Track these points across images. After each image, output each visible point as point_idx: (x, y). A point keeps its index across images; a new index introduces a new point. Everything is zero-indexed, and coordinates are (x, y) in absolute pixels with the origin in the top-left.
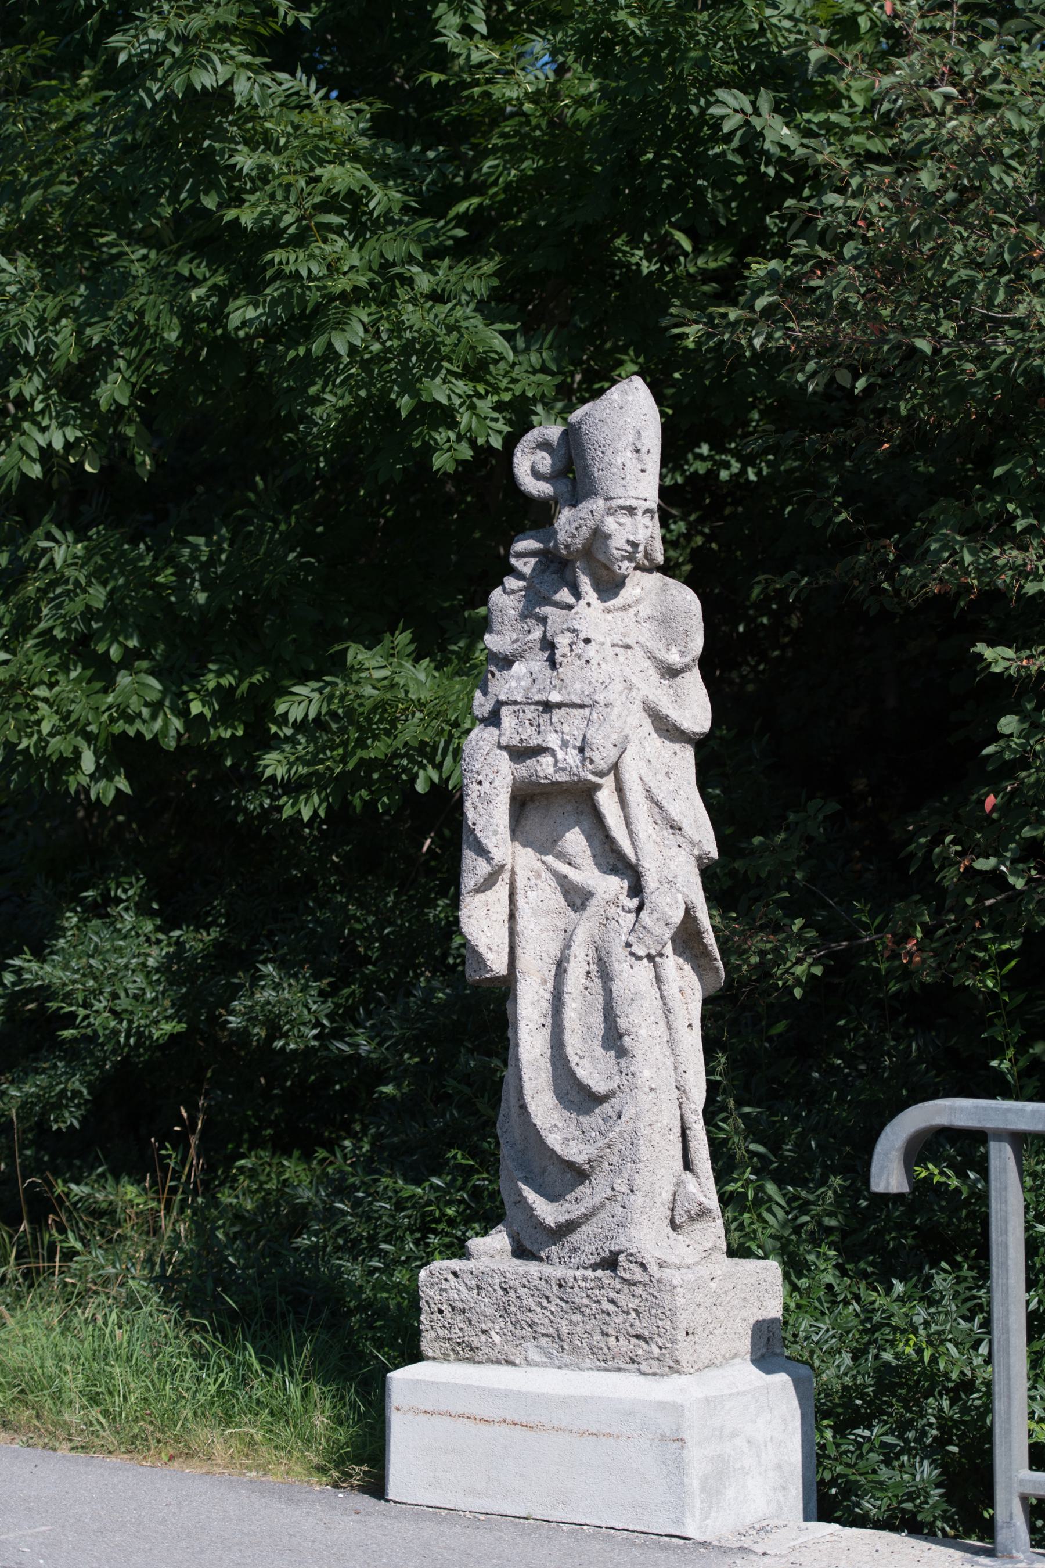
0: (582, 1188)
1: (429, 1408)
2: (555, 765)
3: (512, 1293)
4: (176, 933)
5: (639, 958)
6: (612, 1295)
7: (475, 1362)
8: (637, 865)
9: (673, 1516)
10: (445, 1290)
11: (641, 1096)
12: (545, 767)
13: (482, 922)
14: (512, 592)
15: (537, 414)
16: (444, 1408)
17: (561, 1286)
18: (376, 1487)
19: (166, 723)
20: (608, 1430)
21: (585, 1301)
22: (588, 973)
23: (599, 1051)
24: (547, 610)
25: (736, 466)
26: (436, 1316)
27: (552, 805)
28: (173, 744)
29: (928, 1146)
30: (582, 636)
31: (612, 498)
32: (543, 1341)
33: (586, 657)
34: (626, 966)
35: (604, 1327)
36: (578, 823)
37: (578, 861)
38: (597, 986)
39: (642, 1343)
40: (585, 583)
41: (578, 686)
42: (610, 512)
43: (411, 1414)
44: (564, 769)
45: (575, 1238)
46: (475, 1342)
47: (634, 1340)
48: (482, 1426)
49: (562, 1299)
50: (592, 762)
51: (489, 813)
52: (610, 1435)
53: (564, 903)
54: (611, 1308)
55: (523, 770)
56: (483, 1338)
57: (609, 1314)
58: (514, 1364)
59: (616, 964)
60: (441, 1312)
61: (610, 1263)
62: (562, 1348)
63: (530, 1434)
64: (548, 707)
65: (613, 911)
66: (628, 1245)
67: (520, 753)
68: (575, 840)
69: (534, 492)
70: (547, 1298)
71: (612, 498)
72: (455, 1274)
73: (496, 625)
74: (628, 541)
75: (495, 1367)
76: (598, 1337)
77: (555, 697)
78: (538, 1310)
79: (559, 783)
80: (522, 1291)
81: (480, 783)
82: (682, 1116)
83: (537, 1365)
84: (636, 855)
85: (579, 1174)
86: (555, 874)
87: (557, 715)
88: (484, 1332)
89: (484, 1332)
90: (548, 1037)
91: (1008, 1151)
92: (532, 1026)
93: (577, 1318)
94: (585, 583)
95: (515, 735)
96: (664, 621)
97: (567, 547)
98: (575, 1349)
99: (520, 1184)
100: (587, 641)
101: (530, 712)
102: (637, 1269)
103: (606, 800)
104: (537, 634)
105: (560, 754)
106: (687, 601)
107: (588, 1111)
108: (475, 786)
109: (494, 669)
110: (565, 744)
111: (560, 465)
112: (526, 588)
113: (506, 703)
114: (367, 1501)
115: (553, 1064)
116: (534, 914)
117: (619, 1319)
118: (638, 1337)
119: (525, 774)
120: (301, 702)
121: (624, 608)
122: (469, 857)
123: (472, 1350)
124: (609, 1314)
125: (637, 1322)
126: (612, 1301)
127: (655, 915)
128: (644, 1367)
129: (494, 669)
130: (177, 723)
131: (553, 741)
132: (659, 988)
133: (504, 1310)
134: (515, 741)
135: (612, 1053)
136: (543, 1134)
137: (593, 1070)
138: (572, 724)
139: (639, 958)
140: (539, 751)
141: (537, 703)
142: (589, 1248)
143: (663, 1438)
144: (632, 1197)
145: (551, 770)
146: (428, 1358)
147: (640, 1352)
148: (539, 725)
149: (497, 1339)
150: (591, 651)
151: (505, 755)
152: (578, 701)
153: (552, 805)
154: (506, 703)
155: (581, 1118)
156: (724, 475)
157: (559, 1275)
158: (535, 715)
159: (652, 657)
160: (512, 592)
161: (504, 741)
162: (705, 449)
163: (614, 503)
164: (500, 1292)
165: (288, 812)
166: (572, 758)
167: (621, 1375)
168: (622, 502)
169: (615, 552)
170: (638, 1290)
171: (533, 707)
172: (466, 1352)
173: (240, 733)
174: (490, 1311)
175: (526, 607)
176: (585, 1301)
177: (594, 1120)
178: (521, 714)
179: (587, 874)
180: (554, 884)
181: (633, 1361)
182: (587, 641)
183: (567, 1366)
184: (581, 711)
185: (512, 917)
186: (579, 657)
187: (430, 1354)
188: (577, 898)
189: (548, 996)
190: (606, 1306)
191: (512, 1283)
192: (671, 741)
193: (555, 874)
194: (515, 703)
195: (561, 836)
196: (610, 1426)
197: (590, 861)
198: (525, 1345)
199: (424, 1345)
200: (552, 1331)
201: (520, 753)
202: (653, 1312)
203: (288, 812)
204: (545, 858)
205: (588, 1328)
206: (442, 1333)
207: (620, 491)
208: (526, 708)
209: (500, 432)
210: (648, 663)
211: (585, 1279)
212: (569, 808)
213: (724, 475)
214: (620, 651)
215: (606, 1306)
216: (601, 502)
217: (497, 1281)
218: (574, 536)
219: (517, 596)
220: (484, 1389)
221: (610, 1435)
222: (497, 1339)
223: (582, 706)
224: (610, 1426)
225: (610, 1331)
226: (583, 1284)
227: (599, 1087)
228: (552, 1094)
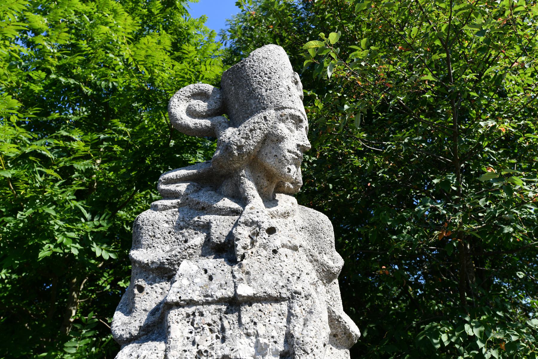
14: (165, 208)
15: (93, 247)
24: (205, 218)
30: (266, 226)
31: (283, 108)
40: (250, 187)
64: (234, 304)
71: (283, 108)
73: (146, 240)
74: (298, 145)
77: (244, 290)
87: (248, 313)
94: (250, 187)
95: (190, 347)
96: (314, 231)
97: (240, 148)
101: (210, 314)
104: (198, 239)
109: (142, 282)
112: (179, 205)
113: (177, 305)
129: (142, 282)
141: (220, 301)
148: (223, 330)
152: (274, 293)
154: (177, 305)
158: (216, 318)
159: (313, 260)
160: (165, 208)
163: (286, 112)
169: (288, 154)
171: (213, 307)
178: (198, 318)
184: (277, 306)
186: (265, 247)
192: (337, 347)
194: (190, 303)
208: (204, 309)
209: (77, 248)
216: (272, 111)
218: (247, 138)
223: (278, 300)
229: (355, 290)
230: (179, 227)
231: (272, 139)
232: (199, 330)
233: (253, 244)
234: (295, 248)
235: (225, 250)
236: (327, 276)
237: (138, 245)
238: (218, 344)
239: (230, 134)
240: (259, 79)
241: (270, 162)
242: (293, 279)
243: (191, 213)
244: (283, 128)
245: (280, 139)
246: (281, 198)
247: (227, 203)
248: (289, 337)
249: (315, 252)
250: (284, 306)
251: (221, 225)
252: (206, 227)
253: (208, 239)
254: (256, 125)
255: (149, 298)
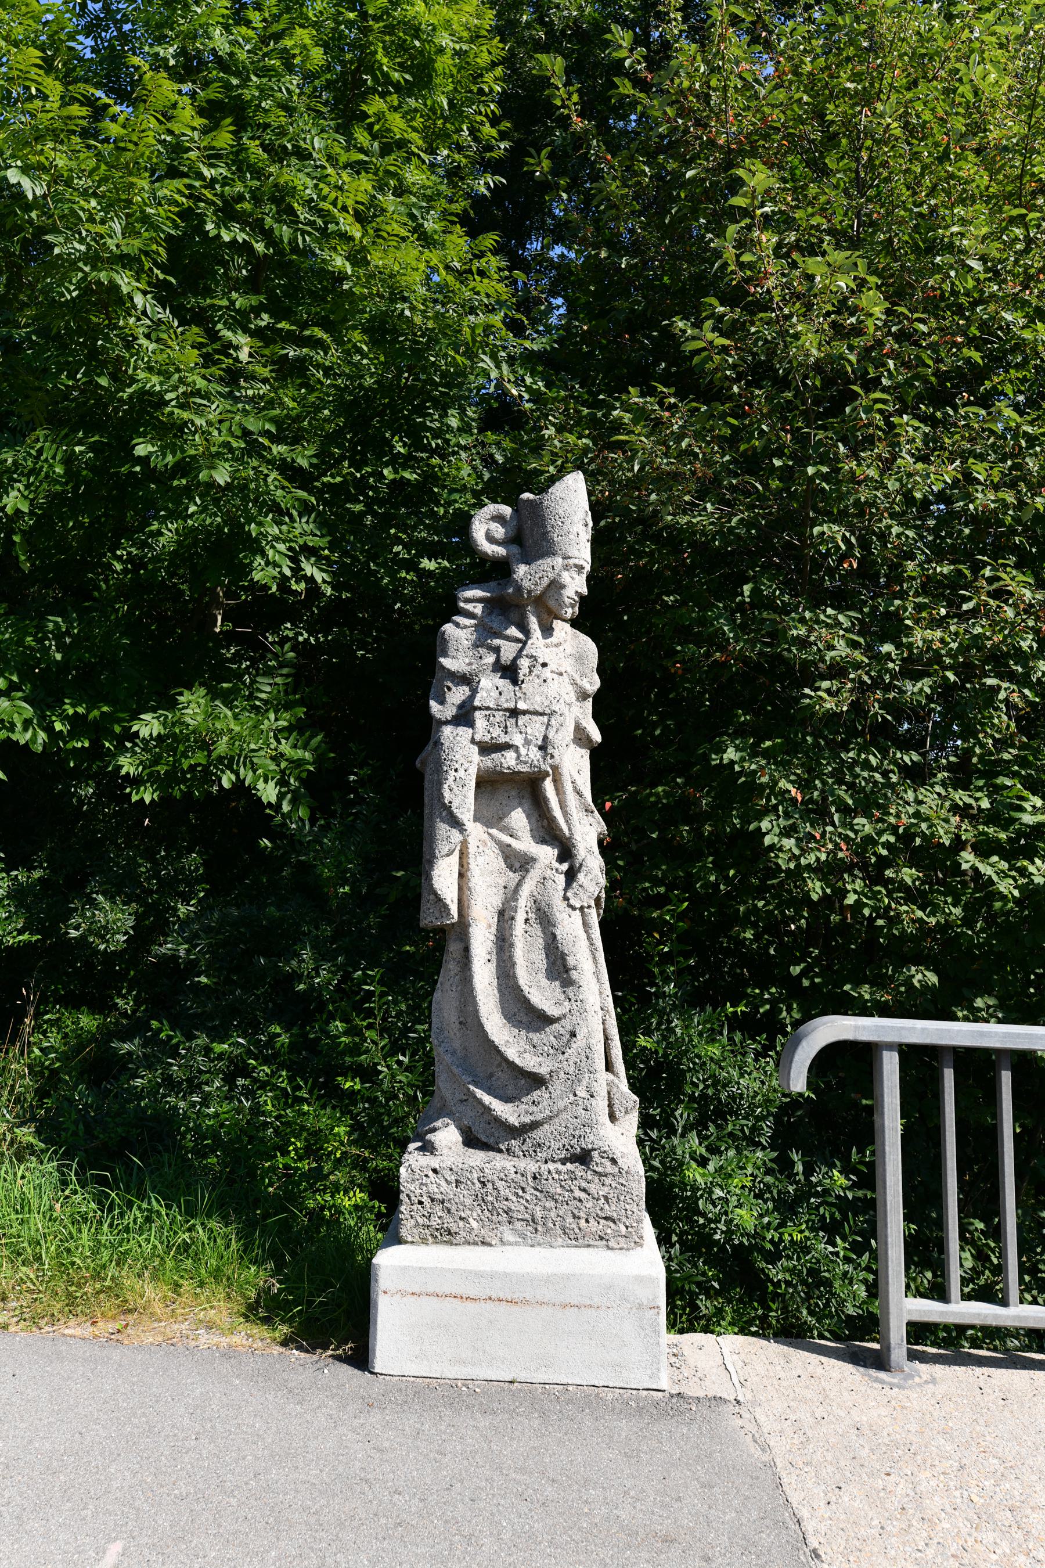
0: (538, 1092)
1: (416, 1290)
2: (518, 758)
3: (490, 1186)
4: (15, 873)
5: (574, 908)
6: (584, 1184)
7: (452, 1244)
8: (570, 838)
9: (649, 1372)
10: (426, 1185)
11: (589, 1018)
12: (509, 759)
13: (444, 878)
14: (465, 627)
16: (431, 1290)
17: (535, 1178)
18: (361, 1359)
19: (35, 735)
20: (588, 1302)
21: (559, 1190)
22: (527, 920)
23: (545, 982)
24: (497, 642)
25: (306, 635)
26: (416, 1207)
27: (514, 789)
28: (40, 748)
29: (834, 1055)
30: (541, 661)
32: (518, 1225)
33: (543, 677)
34: (565, 916)
35: (576, 1212)
36: (520, 805)
37: (519, 834)
38: (536, 930)
39: (611, 1224)
41: (538, 699)
42: (566, 568)
43: (398, 1297)
44: (526, 763)
45: (538, 1134)
46: (454, 1229)
47: (602, 1221)
48: (469, 1304)
49: (536, 1189)
50: (552, 757)
51: (460, 793)
52: (591, 1306)
53: (504, 866)
54: (583, 1195)
55: (488, 762)
56: (461, 1224)
57: (580, 1201)
58: (490, 1245)
59: (558, 915)
60: (421, 1203)
61: (583, 1158)
62: (536, 1230)
63: (515, 1308)
64: (514, 713)
65: (549, 873)
66: (601, 1144)
67: (486, 748)
68: (518, 819)
69: (490, 552)
70: (523, 1189)
72: (435, 1171)
73: (452, 652)
75: (472, 1247)
76: (569, 1219)
77: (522, 706)
78: (514, 1199)
79: (519, 772)
80: (500, 1184)
81: (456, 770)
82: (605, 1030)
83: (510, 1244)
84: (570, 830)
85: (537, 1081)
86: (499, 843)
87: (522, 720)
88: (461, 1218)
89: (461, 1218)
90: (494, 971)
91: (895, 1056)
92: (483, 961)
93: (550, 1204)
97: (529, 592)
98: (548, 1231)
99: (471, 1087)
100: (544, 665)
101: (499, 716)
102: (608, 1163)
103: (548, 785)
104: (490, 659)
105: (523, 751)
106: (590, 647)
107: (538, 1030)
108: (453, 773)
109: (450, 684)
110: (527, 743)
111: (511, 534)
112: (476, 626)
113: (480, 709)
114: (346, 1371)
115: (500, 991)
116: (482, 875)
117: (590, 1205)
118: (606, 1218)
119: (490, 765)
120: (149, 726)
121: (557, 645)
122: (442, 828)
123: (450, 1234)
124: (580, 1201)
125: (606, 1207)
126: (584, 1190)
127: (590, 877)
128: (612, 1244)
129: (450, 684)
130: (42, 736)
131: (518, 740)
132: (586, 932)
133: (481, 1200)
134: (487, 738)
135: (557, 983)
136: (502, 1049)
137: (542, 995)
138: (535, 728)
139: (574, 908)
140: (507, 746)
141: (506, 710)
142: (554, 1145)
143: (640, 1306)
144: (593, 1101)
145: (513, 763)
146: (406, 1242)
147: (609, 1231)
149: (474, 1224)
150: (546, 673)
151: (475, 749)
152: (540, 710)
153: (514, 789)
154: (480, 709)
155: (530, 1035)
156: (301, 639)
157: (533, 1169)
159: (574, 683)
160: (465, 627)
161: (478, 738)
162: (289, 625)
163: (571, 561)
164: (478, 1185)
165: (135, 798)
166: (535, 754)
167: (590, 1250)
168: (577, 561)
170: (608, 1181)
172: (446, 1236)
173: (87, 745)
174: (468, 1201)
175: (478, 639)
176: (559, 1190)
177: (547, 1036)
179: (526, 844)
180: (497, 851)
181: (601, 1238)
182: (544, 665)
183: (539, 1244)
185: (461, 875)
187: (410, 1239)
188: (519, 863)
189: (492, 938)
190: (578, 1193)
191: (490, 1177)
193: (499, 843)
194: (488, 708)
195: (506, 814)
196: (591, 1298)
197: (528, 834)
198: (501, 1228)
199: (403, 1232)
200: (527, 1216)
201: (486, 748)
202: (622, 1198)
203: (135, 798)
204: (491, 831)
205: (561, 1213)
206: (421, 1221)
207: (576, 553)
208: (496, 713)
210: (570, 688)
211: (558, 1172)
212: (513, 793)
213: (301, 639)
214: (555, 676)
215: (578, 1193)
216: (560, 560)
217: (476, 1176)
219: (469, 630)
220: (471, 1272)
221: (591, 1306)
222: (474, 1224)
223: (542, 714)
224: (591, 1298)
225: (582, 1214)
226: (556, 1176)
227: (552, 1011)
228: (500, 1015)
229: (603, 706)
230: (476, 646)
231: (556, 586)
232: (492, 725)
233: (530, 672)
234: (561, 674)
235: (509, 672)
236: (583, 696)
237: (445, 655)
238: (502, 735)
239: (521, 571)
240: (552, 522)
241: (552, 604)
242: (554, 702)
243: (486, 634)
244: (566, 577)
245: (563, 587)
246: (558, 624)
247: (513, 631)
248: (545, 738)
249: (577, 677)
250: (545, 719)
251: (508, 651)
252: (497, 650)
253: (498, 660)
254: (547, 567)
255: (457, 695)
